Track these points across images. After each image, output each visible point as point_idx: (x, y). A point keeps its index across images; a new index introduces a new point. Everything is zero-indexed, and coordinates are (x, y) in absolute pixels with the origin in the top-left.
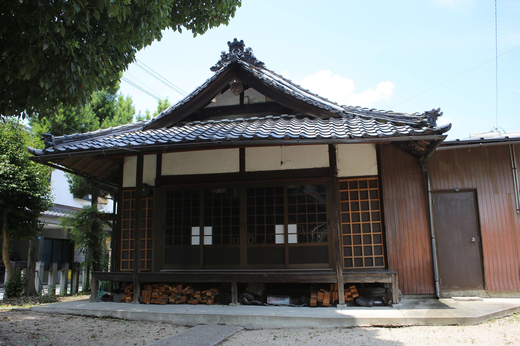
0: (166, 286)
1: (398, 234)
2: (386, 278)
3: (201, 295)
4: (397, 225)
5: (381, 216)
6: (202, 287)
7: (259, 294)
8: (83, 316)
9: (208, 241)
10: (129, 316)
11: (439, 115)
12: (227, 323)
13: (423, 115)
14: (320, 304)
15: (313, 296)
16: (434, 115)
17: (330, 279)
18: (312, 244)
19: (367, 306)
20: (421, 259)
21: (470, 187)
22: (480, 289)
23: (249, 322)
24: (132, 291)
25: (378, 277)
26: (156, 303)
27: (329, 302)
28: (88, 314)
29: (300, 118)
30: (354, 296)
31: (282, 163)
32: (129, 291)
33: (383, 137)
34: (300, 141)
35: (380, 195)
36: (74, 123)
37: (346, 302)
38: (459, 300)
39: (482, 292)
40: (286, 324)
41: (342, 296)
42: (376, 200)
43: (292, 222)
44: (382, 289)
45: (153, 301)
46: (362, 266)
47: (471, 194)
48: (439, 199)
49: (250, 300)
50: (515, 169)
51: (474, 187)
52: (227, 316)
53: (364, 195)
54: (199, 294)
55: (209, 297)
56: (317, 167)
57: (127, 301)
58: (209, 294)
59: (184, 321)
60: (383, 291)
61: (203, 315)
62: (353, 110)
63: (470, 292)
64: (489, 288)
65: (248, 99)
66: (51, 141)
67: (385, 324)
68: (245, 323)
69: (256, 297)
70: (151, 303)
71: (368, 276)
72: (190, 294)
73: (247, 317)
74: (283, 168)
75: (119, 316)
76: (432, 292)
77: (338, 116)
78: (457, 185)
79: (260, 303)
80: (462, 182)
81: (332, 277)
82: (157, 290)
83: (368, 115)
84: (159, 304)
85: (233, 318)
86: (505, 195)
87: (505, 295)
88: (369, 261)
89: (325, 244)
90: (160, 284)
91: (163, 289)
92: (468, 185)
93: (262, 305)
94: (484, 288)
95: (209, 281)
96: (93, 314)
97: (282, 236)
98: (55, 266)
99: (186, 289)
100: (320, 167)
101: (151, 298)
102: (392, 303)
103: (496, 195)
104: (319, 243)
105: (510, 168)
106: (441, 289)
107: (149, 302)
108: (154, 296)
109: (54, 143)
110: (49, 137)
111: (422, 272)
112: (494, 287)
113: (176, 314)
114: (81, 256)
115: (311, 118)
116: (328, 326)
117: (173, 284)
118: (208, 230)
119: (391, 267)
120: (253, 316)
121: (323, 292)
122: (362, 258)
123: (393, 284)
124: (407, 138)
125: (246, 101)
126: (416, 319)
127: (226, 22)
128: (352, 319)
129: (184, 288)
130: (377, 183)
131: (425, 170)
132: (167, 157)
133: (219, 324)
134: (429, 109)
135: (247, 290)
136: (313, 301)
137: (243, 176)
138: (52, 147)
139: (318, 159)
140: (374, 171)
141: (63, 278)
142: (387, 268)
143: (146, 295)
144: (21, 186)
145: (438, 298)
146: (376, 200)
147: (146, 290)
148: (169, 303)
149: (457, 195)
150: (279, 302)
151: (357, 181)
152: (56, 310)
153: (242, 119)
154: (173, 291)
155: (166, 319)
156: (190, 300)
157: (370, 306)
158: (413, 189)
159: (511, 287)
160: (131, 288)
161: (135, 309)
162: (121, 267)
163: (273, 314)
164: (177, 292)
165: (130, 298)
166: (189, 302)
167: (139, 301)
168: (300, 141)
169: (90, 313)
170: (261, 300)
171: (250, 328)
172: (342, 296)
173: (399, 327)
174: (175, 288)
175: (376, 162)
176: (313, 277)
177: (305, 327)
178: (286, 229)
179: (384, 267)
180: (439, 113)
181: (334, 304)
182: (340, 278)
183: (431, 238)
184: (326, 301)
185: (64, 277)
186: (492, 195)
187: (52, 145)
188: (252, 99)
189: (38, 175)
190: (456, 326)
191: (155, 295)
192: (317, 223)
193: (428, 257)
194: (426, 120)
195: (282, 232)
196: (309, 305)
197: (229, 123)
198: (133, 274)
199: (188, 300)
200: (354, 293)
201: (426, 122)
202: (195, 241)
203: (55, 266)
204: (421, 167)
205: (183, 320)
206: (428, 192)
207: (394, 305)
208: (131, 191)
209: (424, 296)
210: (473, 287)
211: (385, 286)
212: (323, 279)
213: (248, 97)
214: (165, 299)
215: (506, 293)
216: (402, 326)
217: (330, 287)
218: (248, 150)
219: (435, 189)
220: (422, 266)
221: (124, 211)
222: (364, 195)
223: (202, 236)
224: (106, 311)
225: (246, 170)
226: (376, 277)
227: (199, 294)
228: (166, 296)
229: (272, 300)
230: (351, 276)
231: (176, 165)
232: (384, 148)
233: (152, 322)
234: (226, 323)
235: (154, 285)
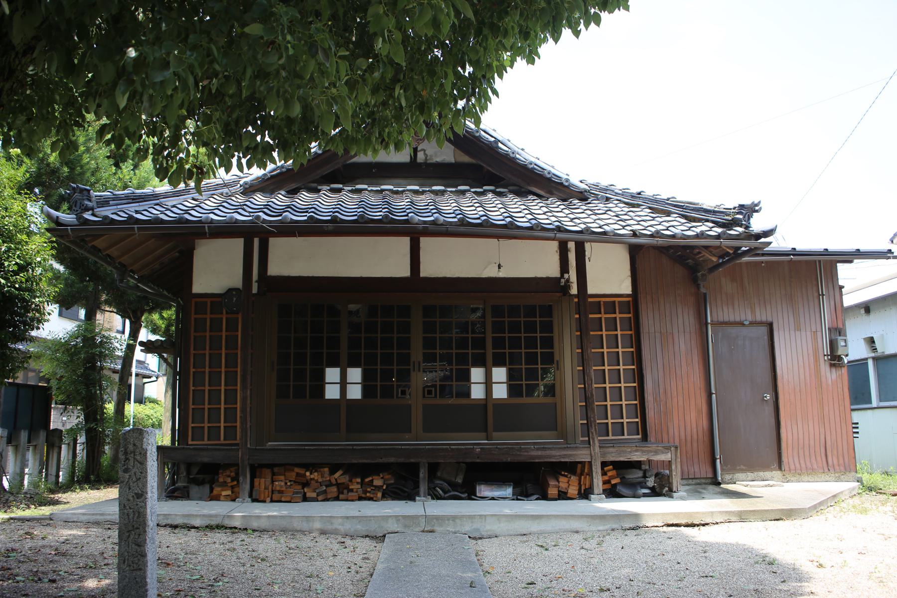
0: (297, 470)
1: (661, 387)
2: (663, 453)
3: (362, 483)
4: (661, 374)
5: (637, 358)
6: (363, 471)
7: (466, 479)
8: (165, 526)
9: (355, 392)
10: (255, 524)
11: (757, 211)
12: (436, 528)
13: (734, 208)
14: (563, 496)
15: (552, 482)
16: (749, 210)
17: (581, 455)
18: (529, 400)
19: (634, 497)
20: (694, 426)
21: (764, 319)
22: (775, 470)
23: (475, 526)
24: (236, 478)
25: (651, 451)
26: (283, 499)
27: (576, 492)
28: (176, 523)
29: (521, 193)
30: (613, 482)
31: (499, 266)
32: (229, 480)
33: (681, 238)
34: (462, 229)
35: (636, 325)
36: (82, 167)
37: (604, 491)
38: (755, 486)
39: (777, 474)
40: (534, 527)
42: (630, 333)
43: (499, 363)
44: (638, 471)
45: (276, 498)
46: (623, 435)
47: (764, 330)
48: (720, 335)
49: (445, 492)
50: (823, 295)
51: (770, 319)
52: (437, 518)
54: (358, 483)
55: (379, 488)
56: (539, 276)
57: (222, 498)
58: (378, 482)
59: (360, 528)
60: (640, 474)
61: (396, 516)
62: (605, 190)
63: (761, 474)
64: (787, 469)
65: (425, 154)
66: (90, 201)
67: (683, 522)
68: (467, 527)
69: (454, 486)
70: (272, 501)
71: (636, 451)
72: (343, 483)
73: (471, 517)
74: (502, 274)
75: (237, 524)
76: (710, 475)
77: (583, 196)
78: (745, 315)
79: (463, 496)
80: (753, 312)
81: (584, 452)
82: (282, 477)
83: (634, 200)
84: (290, 502)
85: (448, 520)
86: (809, 333)
87: (806, 478)
89: (549, 400)
90: (287, 467)
91: (292, 475)
92: (762, 315)
93: (470, 499)
94: (780, 468)
95: (380, 461)
96: (185, 521)
97: (482, 387)
98: (24, 436)
99: (337, 475)
100: (544, 276)
101: (273, 492)
102: (671, 490)
103: (798, 333)
104: (543, 400)
105: (816, 294)
106: (722, 470)
107: (268, 499)
108: (278, 488)
109: (95, 206)
110: (85, 193)
111: (695, 445)
112: (792, 467)
113: (347, 518)
114: (62, 419)
115: (540, 196)
116: (601, 528)
117: (312, 467)
118: (355, 374)
119: (652, 437)
120: (480, 516)
121: (566, 476)
122: (607, 423)
123: (673, 462)
124: (716, 243)
125: (421, 157)
126: (726, 512)
128: (636, 516)
129: (332, 472)
130: (632, 304)
131: (703, 290)
132: (276, 244)
133: (423, 531)
134: (747, 202)
135: (439, 474)
136: (552, 491)
137: (415, 283)
138: (90, 212)
139: (539, 262)
140: (626, 288)
141: (35, 460)
142: (645, 438)
143: (263, 487)
144: (10, 282)
145: (719, 484)
146: (630, 333)
147: (260, 477)
148: (305, 499)
149: (744, 331)
150: (496, 493)
151: (614, 302)
152: (108, 518)
153: (417, 188)
154: (311, 479)
155: (329, 527)
156: (343, 493)
157: (639, 497)
158: (685, 319)
159: (815, 466)
160: (233, 474)
161: (240, 511)
162: (190, 438)
163: (507, 511)
164: (320, 480)
165: (229, 492)
166: (341, 496)
167: (250, 496)
168: (462, 229)
169: (179, 521)
170: (466, 491)
171: (477, 535)
173: (703, 525)
174: (316, 474)
175: (629, 273)
176: (554, 453)
177: (567, 531)
178: (343, 391)
179: (640, 436)
180: (757, 208)
181: (585, 494)
183: (710, 394)
184: (573, 491)
185: (38, 456)
186: (792, 332)
187: (92, 209)
188: (431, 156)
189: (40, 262)
190: (781, 522)
191: (281, 487)
192: (454, 367)
193: (705, 423)
194: (740, 217)
195: (482, 380)
196: (544, 497)
197: (423, 193)
198: (238, 450)
199: (341, 494)
200: (613, 477)
201: (740, 220)
202: (332, 392)
203: (24, 436)
204: (698, 286)
205: (359, 527)
206: (706, 324)
207: (675, 495)
208: (209, 300)
209: (698, 481)
210: (765, 467)
211: (643, 467)
212: (550, 457)
213: (424, 150)
214: (297, 493)
215: (808, 475)
216: (707, 524)
218: (424, 241)
219: (715, 319)
220: (695, 436)
221: (195, 337)
223: (343, 384)
224: (211, 516)
225: (422, 275)
226: (649, 452)
227: (358, 483)
228: (298, 488)
229: (483, 490)
230: (611, 450)
231: (290, 260)
232: (642, 254)
233: (302, 532)
234: (436, 528)
235: (276, 470)
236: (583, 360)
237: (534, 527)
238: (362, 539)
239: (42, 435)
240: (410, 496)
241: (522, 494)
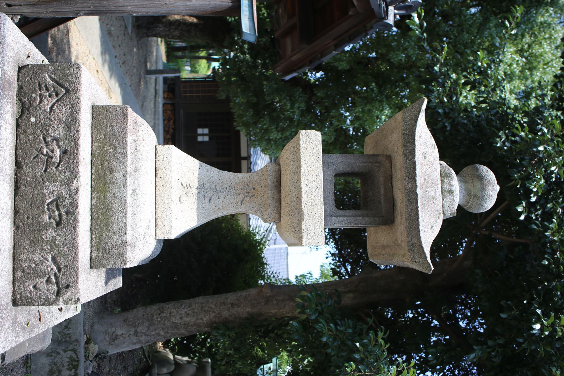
117: (174, 123)
148: (164, 120)
202: (200, 131)
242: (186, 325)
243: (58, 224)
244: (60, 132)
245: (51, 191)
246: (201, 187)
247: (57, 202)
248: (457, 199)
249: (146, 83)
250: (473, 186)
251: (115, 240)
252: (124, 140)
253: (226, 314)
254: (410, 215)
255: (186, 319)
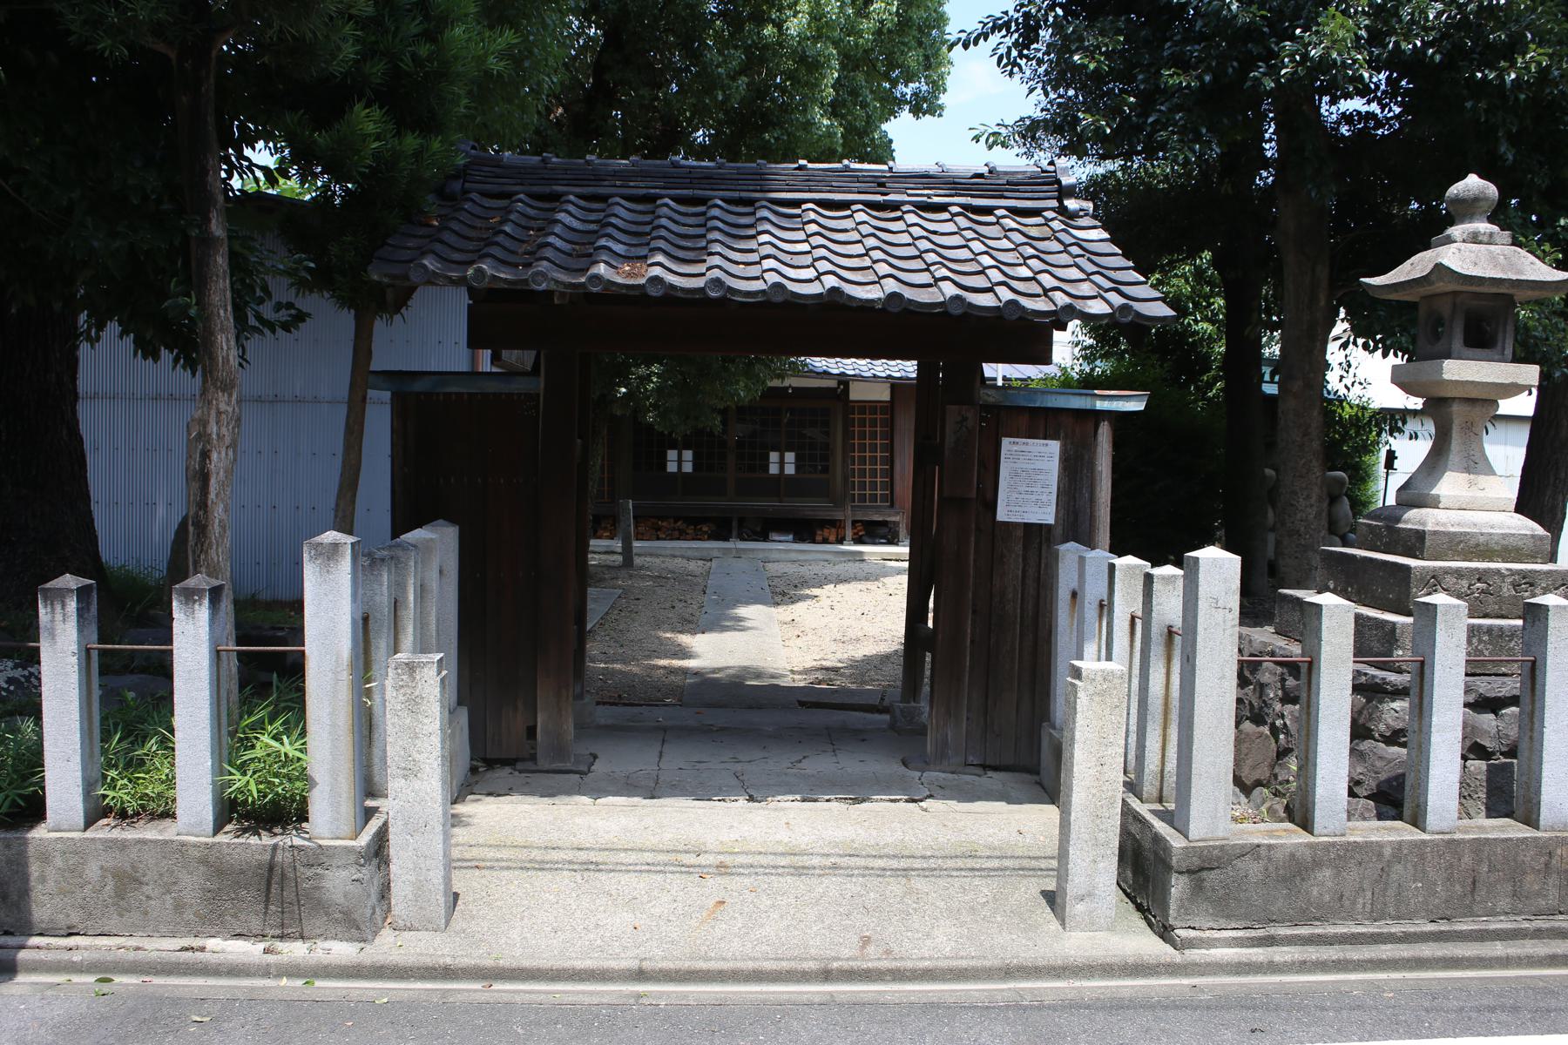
7: (762, 529)
9: (688, 468)
14: (825, 541)
17: (839, 516)
40: (801, 557)
41: (849, 533)
53: (873, 424)
69: (755, 533)
88: (874, 498)
117: (662, 518)
119: (897, 505)
127: (891, 141)
136: (819, 538)
142: (892, 506)
148: (658, 539)
172: (849, 533)
178: (680, 456)
181: (840, 541)
182: (847, 515)
184: (832, 538)
196: (814, 542)
199: (681, 535)
202: (672, 467)
217: (836, 524)
222: (873, 424)
236: (844, 461)
237: (801, 557)
238: (560, 844)
239: (1178, 887)
240: (726, 539)
241: (799, 538)
242: (1320, 500)
243: (1531, 585)
244: (1465, 583)
245: (1507, 590)
246: (1468, 470)
247: (1515, 585)
248: (1483, 227)
249: (641, 568)
250: (1467, 208)
251: (1530, 543)
252: (1455, 534)
253: (1316, 445)
254: (920, 44)
255: (1313, 501)
